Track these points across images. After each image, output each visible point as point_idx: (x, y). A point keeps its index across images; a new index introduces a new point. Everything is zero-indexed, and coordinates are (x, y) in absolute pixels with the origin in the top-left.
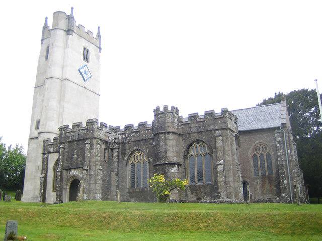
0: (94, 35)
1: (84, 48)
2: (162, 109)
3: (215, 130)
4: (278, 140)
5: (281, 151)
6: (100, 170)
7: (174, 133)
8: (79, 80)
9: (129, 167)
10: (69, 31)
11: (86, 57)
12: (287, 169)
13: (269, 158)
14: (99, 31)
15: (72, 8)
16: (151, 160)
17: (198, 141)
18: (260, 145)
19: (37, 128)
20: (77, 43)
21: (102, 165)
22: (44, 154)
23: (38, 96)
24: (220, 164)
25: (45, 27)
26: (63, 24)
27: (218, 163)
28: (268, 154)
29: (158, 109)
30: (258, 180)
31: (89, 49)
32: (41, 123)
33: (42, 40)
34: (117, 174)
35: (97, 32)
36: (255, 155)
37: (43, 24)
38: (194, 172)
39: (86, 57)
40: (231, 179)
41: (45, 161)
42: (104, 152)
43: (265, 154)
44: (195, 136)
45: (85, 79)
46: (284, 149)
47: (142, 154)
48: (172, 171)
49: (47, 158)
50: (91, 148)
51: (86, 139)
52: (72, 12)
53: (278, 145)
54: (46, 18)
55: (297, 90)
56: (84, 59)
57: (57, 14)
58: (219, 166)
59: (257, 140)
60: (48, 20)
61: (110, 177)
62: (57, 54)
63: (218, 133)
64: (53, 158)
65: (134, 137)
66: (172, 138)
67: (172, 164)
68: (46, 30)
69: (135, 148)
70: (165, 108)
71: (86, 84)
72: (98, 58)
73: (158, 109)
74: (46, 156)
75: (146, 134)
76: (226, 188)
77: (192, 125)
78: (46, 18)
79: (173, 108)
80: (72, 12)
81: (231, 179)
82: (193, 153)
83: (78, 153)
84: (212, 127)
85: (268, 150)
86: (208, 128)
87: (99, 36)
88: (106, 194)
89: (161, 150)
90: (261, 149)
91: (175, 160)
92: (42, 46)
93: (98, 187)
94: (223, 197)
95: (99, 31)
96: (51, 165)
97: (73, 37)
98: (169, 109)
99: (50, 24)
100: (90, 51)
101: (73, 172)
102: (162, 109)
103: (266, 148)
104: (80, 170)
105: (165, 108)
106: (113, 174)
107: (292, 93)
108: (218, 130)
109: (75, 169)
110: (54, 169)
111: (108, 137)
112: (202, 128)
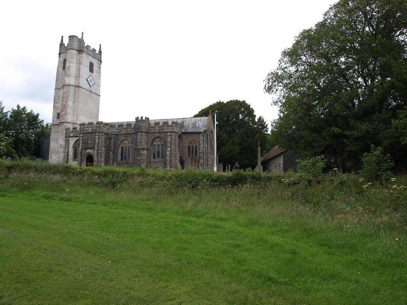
0: (97, 52)
2: (140, 118)
8: (87, 87)
9: (120, 149)
10: (80, 51)
11: (91, 70)
12: (203, 155)
13: (196, 148)
15: (83, 33)
17: (158, 137)
19: (58, 118)
20: (86, 59)
21: (105, 148)
22: (66, 137)
25: (62, 44)
26: (76, 45)
29: (138, 118)
32: (60, 115)
34: (113, 153)
35: (99, 48)
39: (91, 70)
40: (173, 158)
41: (67, 142)
44: (157, 135)
46: (204, 144)
48: (143, 153)
49: (69, 140)
50: (142, 200)
52: (82, 36)
54: (62, 37)
55: (238, 100)
57: (72, 38)
59: (191, 138)
60: (64, 38)
61: (109, 154)
62: (72, 67)
63: (169, 134)
64: (72, 141)
65: (124, 132)
67: (143, 149)
70: (142, 118)
71: (93, 89)
72: (100, 68)
73: (138, 118)
77: (156, 128)
78: (62, 37)
79: (146, 118)
80: (82, 36)
81: (173, 158)
84: (166, 130)
87: (100, 52)
88: (107, 163)
91: (145, 147)
92: (59, 59)
93: (103, 159)
94: (95, 164)
96: (71, 144)
97: (84, 55)
98: (144, 119)
99: (66, 42)
101: (88, 151)
102: (140, 118)
104: (93, 150)
105: (142, 118)
106: (111, 153)
110: (73, 147)
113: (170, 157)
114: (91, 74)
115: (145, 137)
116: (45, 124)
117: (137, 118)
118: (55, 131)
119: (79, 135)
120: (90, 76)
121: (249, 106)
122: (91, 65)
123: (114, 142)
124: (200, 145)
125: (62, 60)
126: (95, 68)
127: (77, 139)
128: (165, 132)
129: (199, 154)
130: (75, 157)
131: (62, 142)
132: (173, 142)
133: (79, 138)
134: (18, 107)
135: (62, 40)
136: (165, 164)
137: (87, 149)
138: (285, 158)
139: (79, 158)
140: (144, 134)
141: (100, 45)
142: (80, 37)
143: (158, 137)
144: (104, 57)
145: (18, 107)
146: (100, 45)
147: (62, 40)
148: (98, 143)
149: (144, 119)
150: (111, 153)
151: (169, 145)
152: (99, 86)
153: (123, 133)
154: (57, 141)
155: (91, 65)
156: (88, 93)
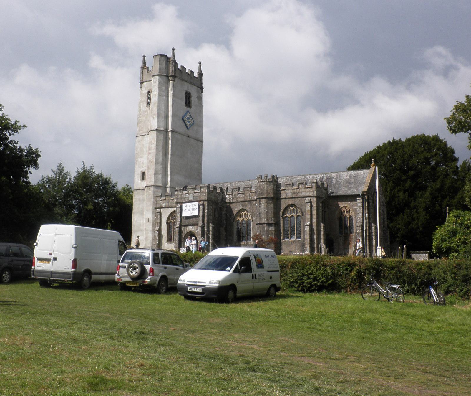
1: (186, 93)
3: (306, 197)
5: (360, 215)
11: (188, 103)
14: (200, 67)
16: (254, 218)
18: (346, 208)
24: (307, 225)
25: (144, 67)
27: (306, 224)
28: (351, 216)
29: (18, 122)
30: (341, 238)
31: (191, 92)
33: (141, 83)
38: (288, 227)
39: (188, 103)
42: (215, 212)
43: (348, 216)
44: (290, 202)
45: (188, 127)
47: (246, 213)
49: (160, 213)
52: (173, 54)
53: (358, 209)
55: (426, 135)
56: (186, 105)
68: (145, 71)
69: (241, 208)
71: (190, 132)
72: (200, 99)
73: (18, 122)
74: (158, 210)
75: (250, 196)
76: (107, 330)
80: (173, 54)
84: (303, 194)
86: (300, 195)
87: (201, 74)
89: (262, 212)
95: (200, 67)
100: (192, 95)
103: (349, 211)
104: (196, 227)
106: (222, 230)
107: (414, 137)
109: (191, 225)
110: (167, 223)
111: (218, 197)
112: (295, 195)
114: (188, 109)
116: (469, 136)
118: (139, 200)
119: (174, 205)
121: (445, 144)
122: (188, 96)
124: (356, 214)
125: (145, 91)
126: (194, 99)
127: (172, 210)
128: (302, 197)
129: (356, 229)
130: (170, 239)
131: (149, 215)
133: (175, 209)
135: (144, 62)
136: (303, 245)
137: (187, 226)
139: (177, 238)
141: (200, 63)
142: (170, 55)
143: (292, 205)
146: (200, 63)
147: (144, 62)
150: (222, 230)
152: (201, 126)
153: (239, 200)
154: (142, 213)
155: (188, 96)
156: (185, 138)
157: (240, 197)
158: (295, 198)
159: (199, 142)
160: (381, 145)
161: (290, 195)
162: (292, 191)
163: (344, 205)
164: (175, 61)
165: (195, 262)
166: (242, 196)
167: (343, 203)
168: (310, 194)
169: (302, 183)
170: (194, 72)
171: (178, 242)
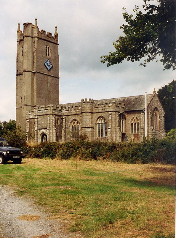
4: (142, 116)
6: (55, 130)
7: (90, 112)
18: (135, 118)
23: (19, 81)
36: (132, 123)
37: (17, 30)
43: (136, 123)
44: (100, 114)
45: (49, 69)
51: (48, 115)
55: (161, 88)
58: (109, 129)
63: (64, 117)
66: (89, 114)
70: (86, 100)
80: (23, 163)
82: (99, 122)
83: (44, 121)
84: (107, 110)
85: (138, 121)
86: (106, 110)
87: (56, 36)
90: (135, 120)
91: (90, 125)
98: (88, 100)
104: (46, 130)
108: (28, 119)
113: (111, 134)
115: (90, 117)
117: (82, 100)
120: (50, 69)
123: (65, 122)
132: (114, 121)
134: (126, 16)
135: (19, 28)
138: (38, 59)
140: (89, 114)
144: (60, 40)
145: (126, 16)
147: (19, 28)
148: (50, 124)
149: (88, 100)
151: (110, 123)
153: (73, 114)
157: (73, 112)
158: (103, 112)
159: (57, 79)
160: (114, 64)
161: (100, 111)
162: (101, 108)
163: (134, 116)
164: (37, 27)
165: (87, 143)
166: (74, 111)
167: (134, 115)
168: (111, 110)
169: (107, 103)
170: (45, 32)
171: (163, 123)
